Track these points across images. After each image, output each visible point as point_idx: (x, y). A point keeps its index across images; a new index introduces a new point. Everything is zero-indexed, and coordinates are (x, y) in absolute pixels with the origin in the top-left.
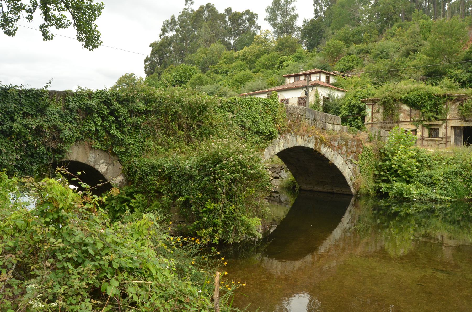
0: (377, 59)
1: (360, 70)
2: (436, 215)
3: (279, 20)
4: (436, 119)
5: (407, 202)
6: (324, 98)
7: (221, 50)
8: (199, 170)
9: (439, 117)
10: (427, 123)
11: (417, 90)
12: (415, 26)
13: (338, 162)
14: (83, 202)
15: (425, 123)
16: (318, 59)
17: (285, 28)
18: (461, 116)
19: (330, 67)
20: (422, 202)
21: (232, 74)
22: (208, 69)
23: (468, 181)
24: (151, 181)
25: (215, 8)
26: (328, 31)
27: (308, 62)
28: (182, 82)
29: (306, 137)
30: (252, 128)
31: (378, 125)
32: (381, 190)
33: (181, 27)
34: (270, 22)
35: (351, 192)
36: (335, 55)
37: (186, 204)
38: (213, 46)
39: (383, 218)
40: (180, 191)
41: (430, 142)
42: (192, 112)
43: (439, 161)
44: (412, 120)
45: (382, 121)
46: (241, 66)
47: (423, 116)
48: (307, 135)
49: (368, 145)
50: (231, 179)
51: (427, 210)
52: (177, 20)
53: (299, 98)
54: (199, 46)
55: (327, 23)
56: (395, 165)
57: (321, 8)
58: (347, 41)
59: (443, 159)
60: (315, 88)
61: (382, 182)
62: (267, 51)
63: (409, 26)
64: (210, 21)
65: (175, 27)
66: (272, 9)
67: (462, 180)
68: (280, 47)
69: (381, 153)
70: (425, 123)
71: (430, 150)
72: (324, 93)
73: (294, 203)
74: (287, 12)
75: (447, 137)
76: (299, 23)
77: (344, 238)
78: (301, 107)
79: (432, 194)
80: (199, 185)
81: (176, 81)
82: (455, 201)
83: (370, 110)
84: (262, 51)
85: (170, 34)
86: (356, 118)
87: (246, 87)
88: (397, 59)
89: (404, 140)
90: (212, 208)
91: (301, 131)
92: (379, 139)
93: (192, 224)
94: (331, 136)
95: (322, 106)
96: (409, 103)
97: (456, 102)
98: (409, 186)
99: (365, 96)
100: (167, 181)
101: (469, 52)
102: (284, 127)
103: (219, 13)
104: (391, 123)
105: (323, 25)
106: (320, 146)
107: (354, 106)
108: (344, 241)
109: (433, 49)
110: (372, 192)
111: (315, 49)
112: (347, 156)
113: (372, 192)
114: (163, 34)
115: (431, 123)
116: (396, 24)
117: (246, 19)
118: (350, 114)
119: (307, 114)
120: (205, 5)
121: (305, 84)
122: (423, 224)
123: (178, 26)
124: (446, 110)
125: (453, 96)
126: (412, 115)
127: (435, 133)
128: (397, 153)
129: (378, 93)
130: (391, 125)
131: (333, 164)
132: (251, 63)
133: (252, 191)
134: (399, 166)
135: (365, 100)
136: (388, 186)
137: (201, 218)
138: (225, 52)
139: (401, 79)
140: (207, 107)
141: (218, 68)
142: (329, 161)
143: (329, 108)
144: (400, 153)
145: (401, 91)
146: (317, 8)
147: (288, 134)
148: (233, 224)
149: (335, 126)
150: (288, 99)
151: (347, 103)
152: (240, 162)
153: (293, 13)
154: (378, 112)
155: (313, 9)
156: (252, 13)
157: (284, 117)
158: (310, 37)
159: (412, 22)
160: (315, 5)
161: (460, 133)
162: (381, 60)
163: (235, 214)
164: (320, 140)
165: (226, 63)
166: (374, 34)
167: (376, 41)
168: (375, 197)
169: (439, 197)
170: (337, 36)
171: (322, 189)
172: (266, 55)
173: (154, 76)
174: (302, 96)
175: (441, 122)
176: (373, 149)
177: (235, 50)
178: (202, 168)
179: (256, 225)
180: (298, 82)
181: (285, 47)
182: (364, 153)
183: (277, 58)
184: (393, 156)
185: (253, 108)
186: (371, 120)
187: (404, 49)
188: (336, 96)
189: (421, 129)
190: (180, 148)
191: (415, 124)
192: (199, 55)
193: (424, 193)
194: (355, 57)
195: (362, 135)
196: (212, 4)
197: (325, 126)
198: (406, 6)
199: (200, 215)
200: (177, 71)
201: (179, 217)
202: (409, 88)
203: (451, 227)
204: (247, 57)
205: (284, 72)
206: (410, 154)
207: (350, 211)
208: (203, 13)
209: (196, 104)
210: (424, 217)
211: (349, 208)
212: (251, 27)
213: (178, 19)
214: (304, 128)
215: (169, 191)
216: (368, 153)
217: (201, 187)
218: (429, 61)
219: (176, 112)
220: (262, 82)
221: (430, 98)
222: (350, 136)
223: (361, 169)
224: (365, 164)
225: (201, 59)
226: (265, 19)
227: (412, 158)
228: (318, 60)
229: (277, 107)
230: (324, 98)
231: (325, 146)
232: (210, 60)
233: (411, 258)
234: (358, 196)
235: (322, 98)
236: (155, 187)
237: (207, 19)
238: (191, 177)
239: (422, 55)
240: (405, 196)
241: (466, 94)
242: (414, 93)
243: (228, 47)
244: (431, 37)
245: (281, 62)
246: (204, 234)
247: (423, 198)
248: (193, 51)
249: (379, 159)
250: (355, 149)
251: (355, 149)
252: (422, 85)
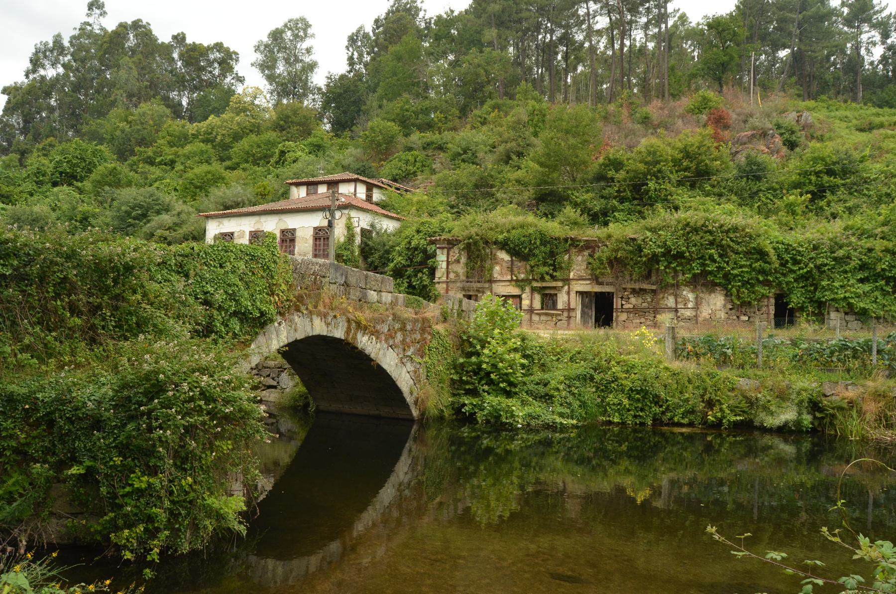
0: (457, 162)
1: (427, 179)
2: (554, 450)
3: (281, 68)
4: (553, 277)
5: (507, 430)
6: (363, 231)
7: (162, 117)
8: (115, 407)
9: (557, 274)
10: (539, 285)
11: (522, 227)
12: (520, 111)
13: (388, 361)
15: (535, 284)
16: (352, 153)
17: (292, 85)
18: (591, 275)
19: (373, 169)
20: (531, 430)
21: (182, 168)
22: (133, 153)
23: (602, 391)
24: (6, 429)
25: (150, 31)
26: (372, 101)
27: (333, 157)
28: (74, 177)
29: (330, 319)
30: (226, 307)
31: (458, 284)
32: (463, 410)
33: (75, 61)
34: (263, 71)
35: (411, 414)
36: (383, 149)
37: (88, 477)
38: (144, 107)
39: (468, 457)
40: (73, 451)
41: (543, 318)
42: (100, 277)
43: (559, 355)
44: (515, 278)
45: (464, 278)
46: (202, 152)
47: (532, 271)
48: (332, 314)
49: (440, 328)
50: (185, 427)
51: (540, 442)
52: (66, 43)
53: (315, 228)
54: (113, 104)
55: (369, 86)
56: (487, 363)
57: (361, 55)
58: (405, 124)
59: (564, 351)
60: (346, 212)
61: (466, 394)
62: (256, 129)
63: (512, 108)
64: (140, 56)
65: (61, 58)
66: (266, 46)
67: (594, 390)
68: (282, 122)
69: (463, 341)
70: (535, 284)
71: (543, 334)
72: (362, 221)
73: (306, 438)
74: (295, 56)
75: (570, 310)
76: (319, 79)
77: (400, 501)
78: (321, 261)
79: (549, 414)
80: (115, 439)
81: (61, 173)
82: (583, 426)
83: (444, 258)
84: (245, 128)
85: (50, 72)
86: (420, 271)
87: (212, 198)
88: (490, 166)
89: (502, 319)
90: (143, 486)
91: (321, 308)
92: (459, 315)
93: (101, 520)
94: (376, 315)
95: (359, 246)
96: (510, 248)
97: (583, 250)
98: (510, 402)
99: (435, 232)
100: (44, 430)
101: (603, 164)
102: (288, 300)
103: (160, 41)
104: (479, 282)
105: (362, 87)
106: (356, 334)
107: (416, 249)
108: (400, 507)
109: (548, 155)
110: (447, 413)
111: (347, 133)
112: (404, 350)
113: (447, 413)
114: (34, 71)
115: (544, 284)
116: (490, 102)
117: (215, 60)
118: (408, 263)
119: (331, 275)
120: (129, 23)
121: (328, 202)
122: (533, 464)
123: (69, 57)
124: (569, 263)
125: (580, 241)
126: (515, 269)
127: (550, 302)
128: (489, 343)
129: (459, 227)
130: (479, 285)
131: (379, 366)
132: (223, 150)
133: (226, 446)
134: (494, 366)
135: (436, 240)
136: (475, 401)
137: (120, 507)
138: (170, 122)
139: (497, 201)
140: (133, 267)
141: (155, 153)
142: (372, 360)
143: (371, 249)
144: (494, 342)
145: (497, 227)
146: (353, 54)
147: (295, 314)
148: (188, 514)
149: (385, 294)
150: (294, 230)
151: (403, 243)
152: (202, 393)
153: (307, 59)
154: (458, 261)
155: (346, 57)
156: (228, 48)
157: (288, 282)
158: (337, 107)
159: (515, 102)
160: (351, 49)
161: (591, 301)
162: (463, 165)
163: (192, 494)
164: (356, 322)
165: (171, 144)
166: (453, 115)
167: (455, 129)
168: (452, 421)
169: (558, 420)
170: (387, 113)
171: (359, 409)
172: (253, 137)
173: (11, 160)
174: (322, 225)
175: (560, 284)
176: (450, 334)
177: (191, 120)
178: (122, 403)
179: (232, 504)
180: (314, 197)
181: (291, 124)
182: (434, 342)
183: (274, 144)
184: (483, 347)
185: (228, 267)
186: (445, 275)
187: (501, 148)
188: (385, 227)
189: (529, 294)
190: (73, 353)
191: (518, 286)
192: (114, 122)
193: (534, 414)
194: (420, 155)
195: (432, 310)
196: (144, 23)
197: (365, 296)
198: (506, 72)
199: (117, 501)
200: (62, 153)
201: (71, 505)
202: (511, 222)
203: (579, 470)
204: (216, 137)
205: (286, 171)
206: (511, 344)
207: (410, 451)
208: (124, 38)
209: (110, 261)
210: (536, 455)
211: (407, 445)
212: (225, 77)
213: (71, 42)
214: (327, 301)
215: (47, 451)
216: (441, 342)
217: (121, 443)
218: (543, 174)
219: (65, 279)
220: (245, 190)
221: (544, 243)
222: (408, 314)
223: (428, 372)
224: (436, 362)
225: (118, 133)
226: (252, 65)
227: (516, 350)
228: (351, 155)
229: (275, 262)
230: (362, 230)
231: (364, 334)
232: (136, 136)
233: (513, 522)
234: (424, 422)
235: (358, 230)
236: (14, 444)
237: (133, 51)
238: (97, 423)
239: (531, 164)
240: (504, 420)
241: (599, 238)
242: (518, 231)
243: (176, 110)
244: (545, 134)
245: (283, 153)
246: (128, 540)
247: (533, 423)
248: (101, 113)
249: (460, 352)
250: (418, 336)
251: (418, 336)
252: (531, 218)
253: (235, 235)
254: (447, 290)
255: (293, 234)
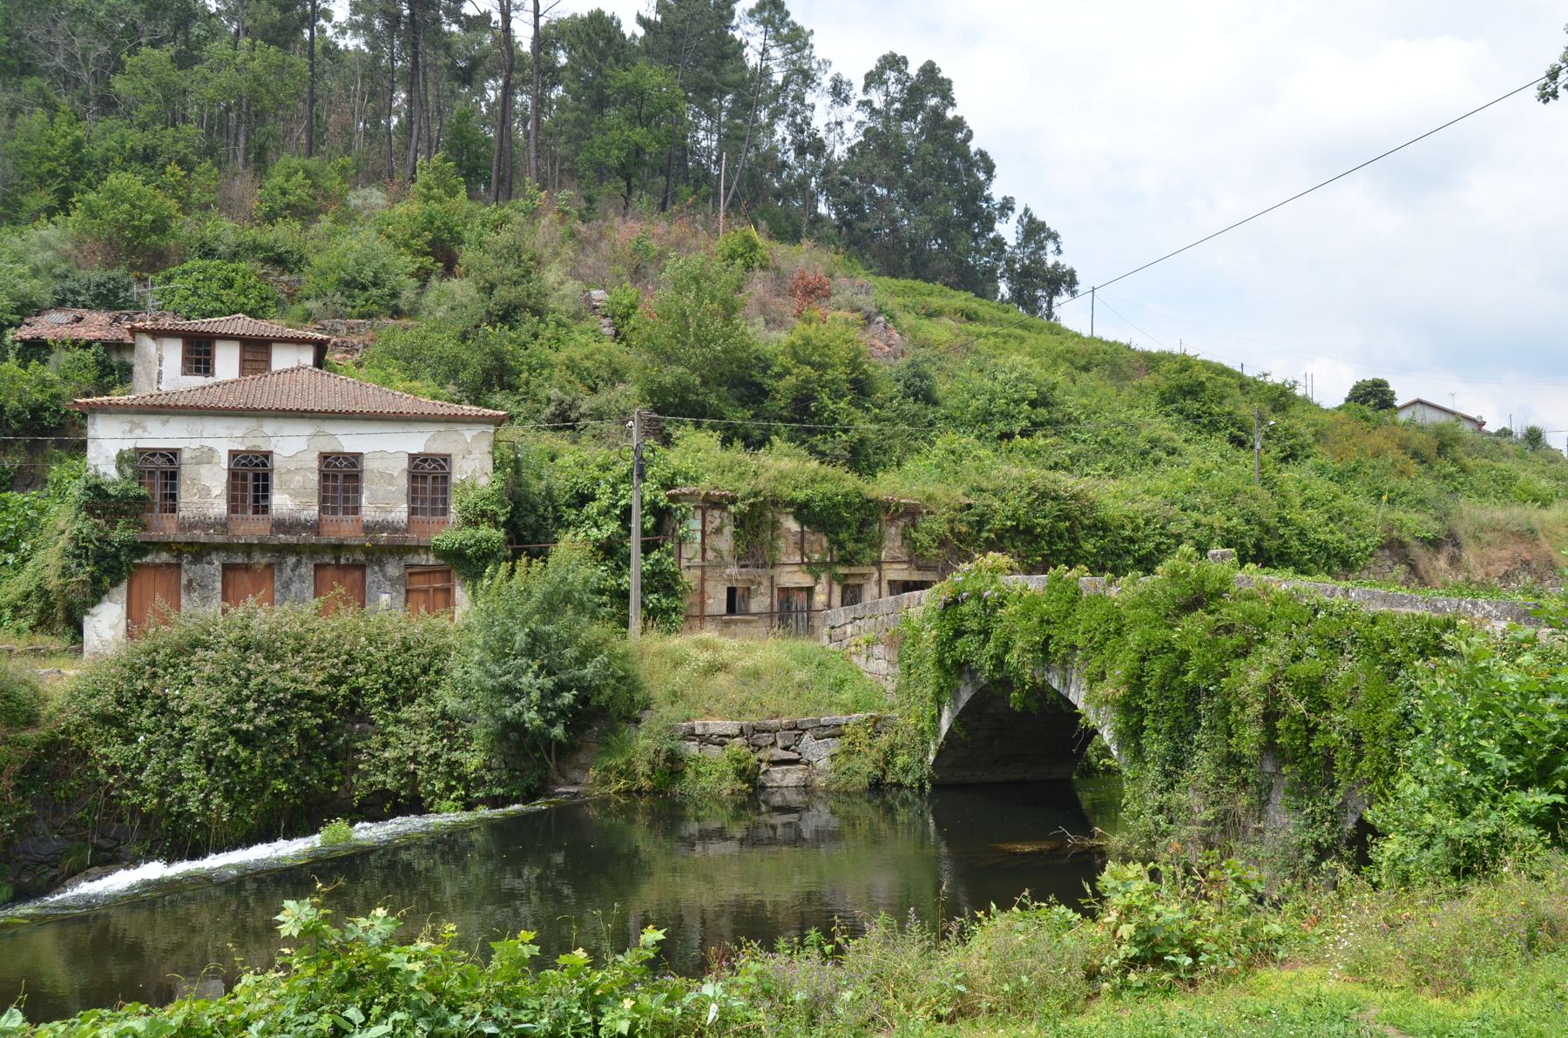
14: (1159, 882)
53: (412, 457)
150: (358, 457)
186: (699, 555)
191: (811, 572)
253: (185, 456)
254: (703, 580)
255: (354, 465)
